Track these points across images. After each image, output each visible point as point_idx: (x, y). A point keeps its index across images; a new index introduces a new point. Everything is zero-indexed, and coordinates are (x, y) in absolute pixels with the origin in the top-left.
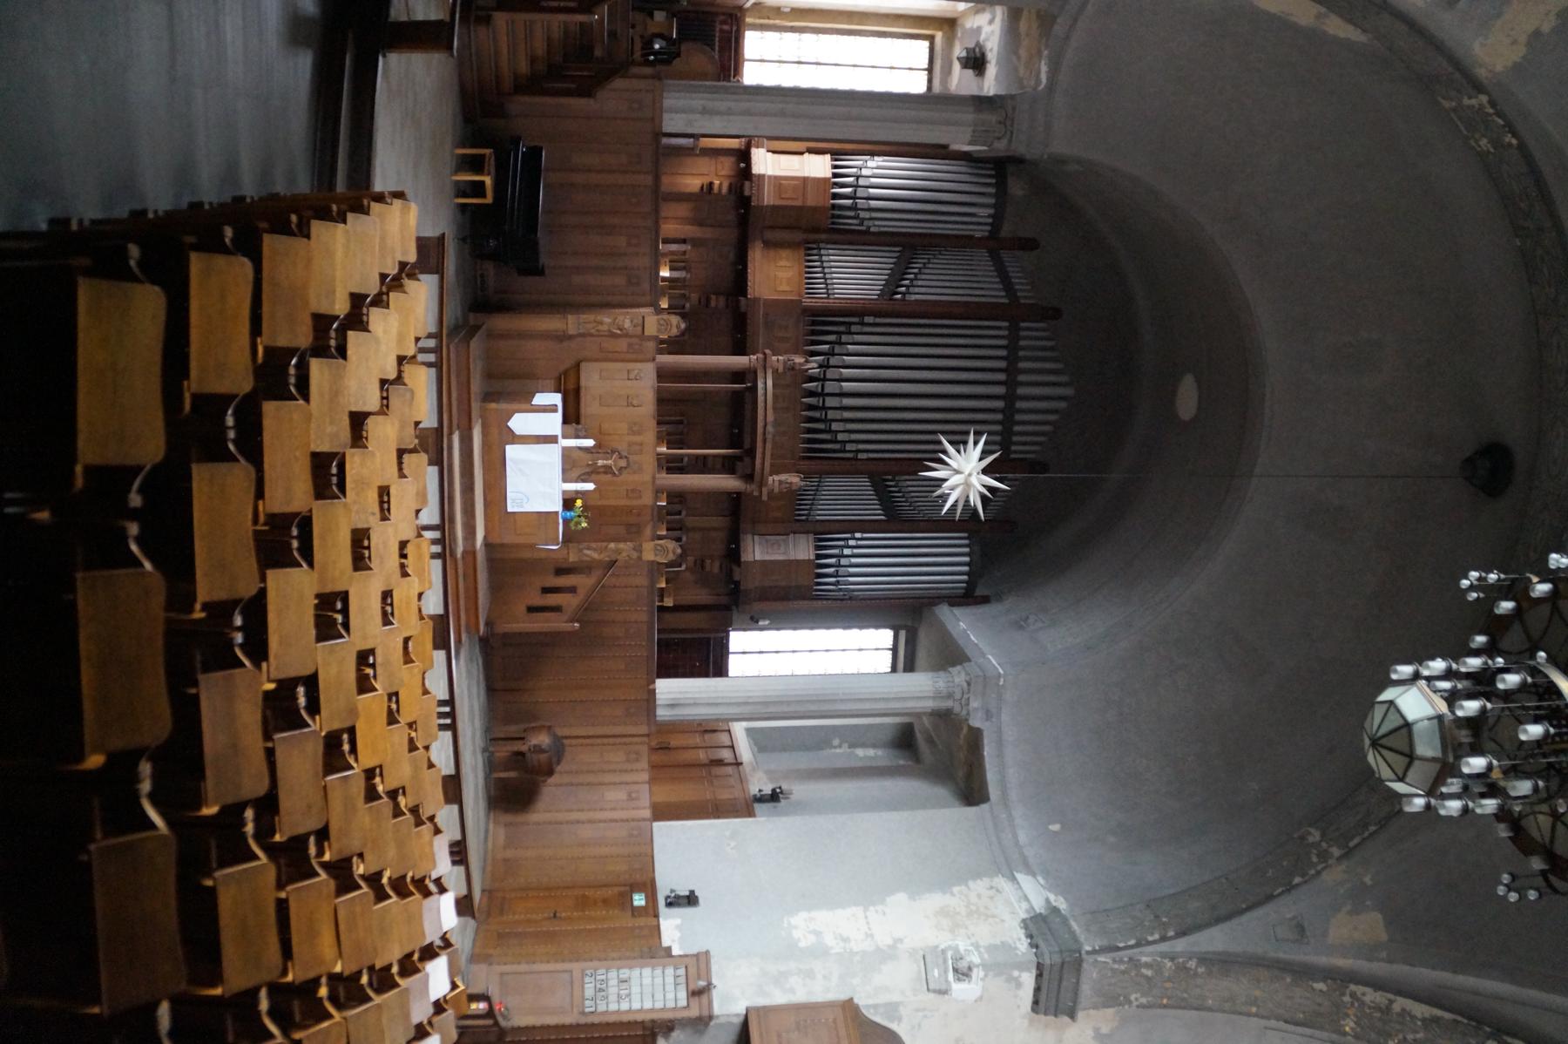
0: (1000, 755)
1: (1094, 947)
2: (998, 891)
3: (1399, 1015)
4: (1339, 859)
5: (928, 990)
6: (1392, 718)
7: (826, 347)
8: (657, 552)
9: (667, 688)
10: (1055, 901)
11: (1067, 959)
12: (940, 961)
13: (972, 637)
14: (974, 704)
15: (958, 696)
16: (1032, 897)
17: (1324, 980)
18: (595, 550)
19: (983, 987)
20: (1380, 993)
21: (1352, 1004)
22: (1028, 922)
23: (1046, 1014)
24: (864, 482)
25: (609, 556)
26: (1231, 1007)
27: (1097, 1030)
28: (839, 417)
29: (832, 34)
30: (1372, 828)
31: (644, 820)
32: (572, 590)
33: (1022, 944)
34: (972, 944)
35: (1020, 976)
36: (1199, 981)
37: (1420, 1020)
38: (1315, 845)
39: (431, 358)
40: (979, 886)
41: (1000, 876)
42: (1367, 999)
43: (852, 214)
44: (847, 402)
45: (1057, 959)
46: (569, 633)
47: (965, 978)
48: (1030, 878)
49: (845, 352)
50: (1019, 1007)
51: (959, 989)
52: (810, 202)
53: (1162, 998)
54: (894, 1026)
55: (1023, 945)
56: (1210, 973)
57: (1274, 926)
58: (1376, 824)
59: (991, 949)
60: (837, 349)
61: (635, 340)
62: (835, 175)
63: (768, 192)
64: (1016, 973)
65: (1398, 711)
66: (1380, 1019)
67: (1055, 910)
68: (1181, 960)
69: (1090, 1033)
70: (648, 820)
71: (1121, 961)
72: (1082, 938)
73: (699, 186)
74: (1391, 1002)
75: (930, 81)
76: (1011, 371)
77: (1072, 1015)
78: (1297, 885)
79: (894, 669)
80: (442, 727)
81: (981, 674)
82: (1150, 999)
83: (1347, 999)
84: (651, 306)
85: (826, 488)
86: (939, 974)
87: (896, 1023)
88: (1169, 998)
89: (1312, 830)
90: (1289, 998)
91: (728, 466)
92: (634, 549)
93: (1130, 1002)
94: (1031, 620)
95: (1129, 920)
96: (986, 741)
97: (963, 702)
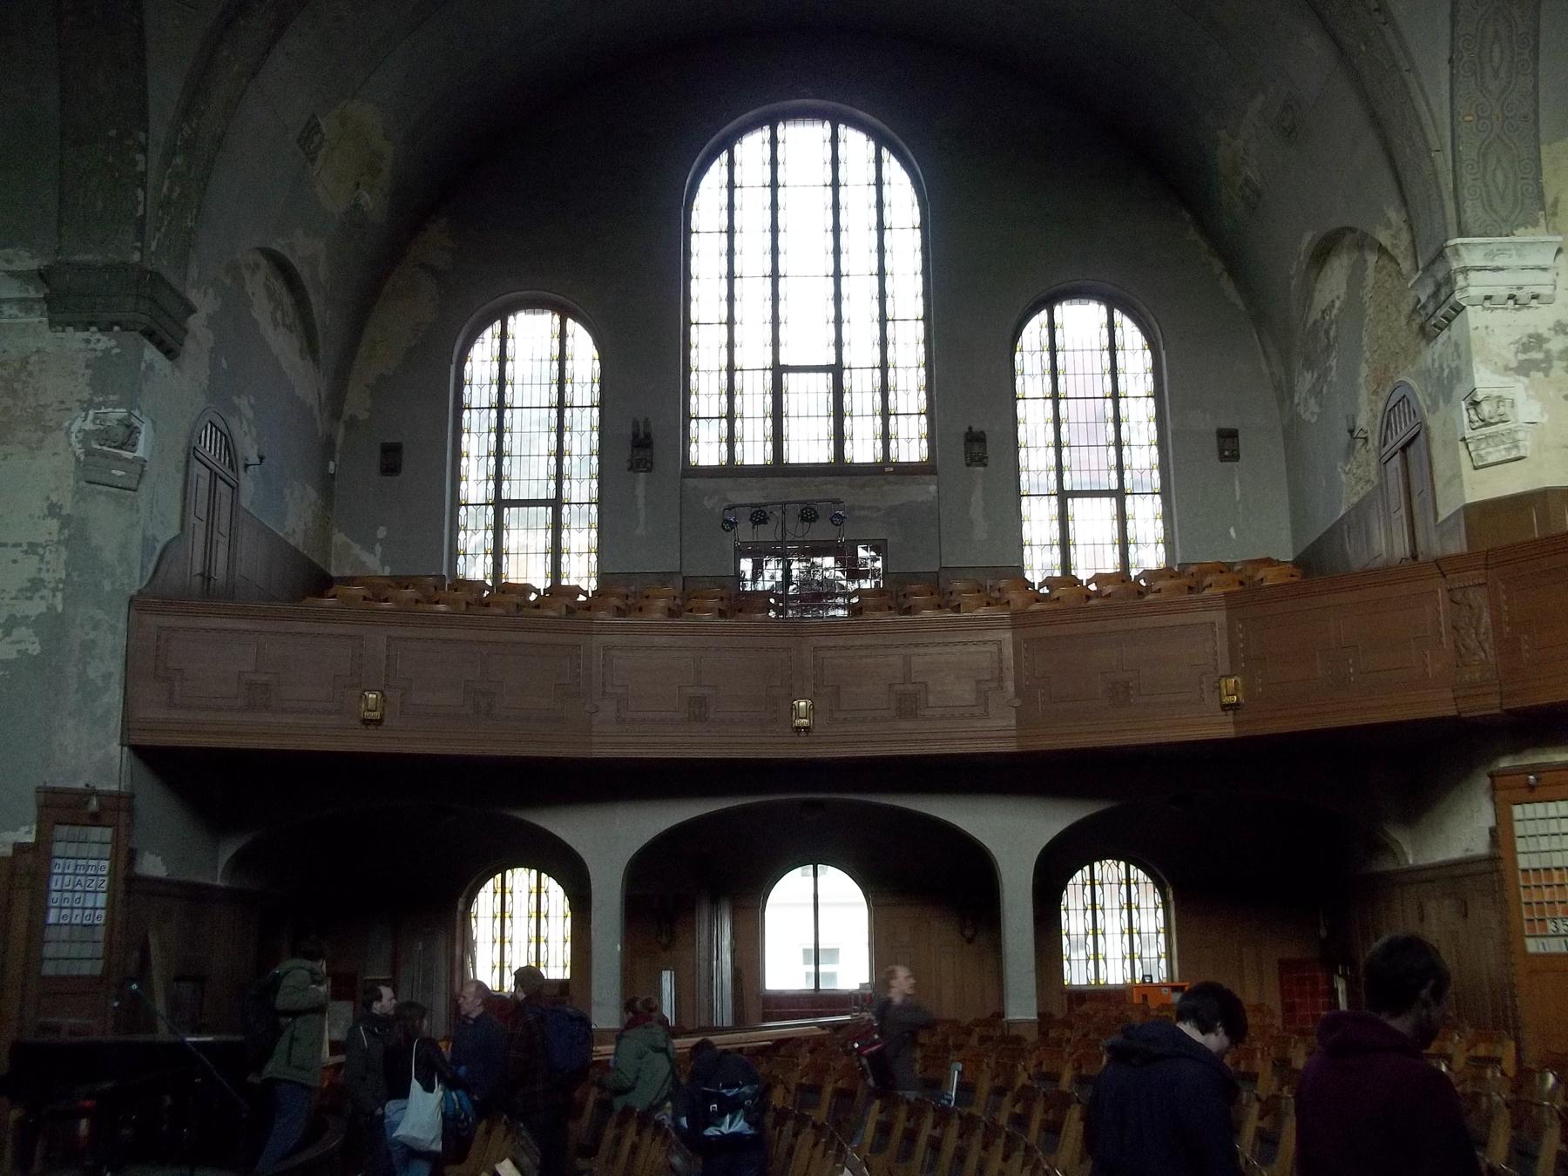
5: (135, 490)
29: (877, 193)
47: (133, 436)
54: (528, 582)
84: (1497, 823)
87: (156, 544)
95: (371, 206)
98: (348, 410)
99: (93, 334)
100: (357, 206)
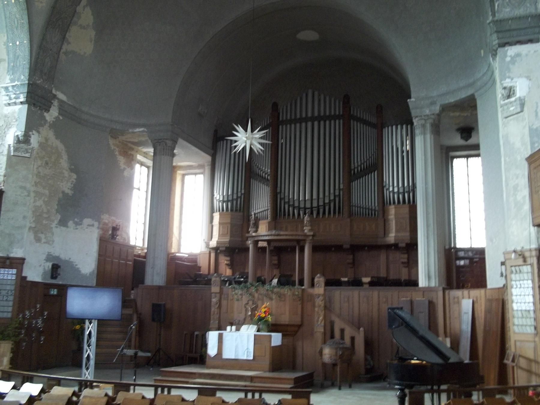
7: (291, 209)
8: (320, 286)
9: (422, 282)
12: (505, 107)
14: (427, 112)
15: (423, 122)
18: (319, 318)
19: (519, 77)
24: (354, 184)
25: (322, 311)
28: (322, 200)
31: (485, 292)
32: (342, 331)
39: (166, 390)
43: (235, 202)
44: (315, 196)
46: (365, 333)
47: (512, 90)
49: (292, 199)
50: (535, 52)
51: (519, 93)
52: (229, 221)
60: (291, 203)
61: (223, 296)
62: (219, 211)
63: (224, 239)
64: (508, 59)
70: (486, 291)
73: (229, 270)
75: (199, 173)
76: (301, 120)
79: (478, 155)
80: (169, 392)
85: (367, 204)
86: (512, 106)
91: (302, 250)
92: (318, 297)
96: (447, 102)
97: (426, 118)
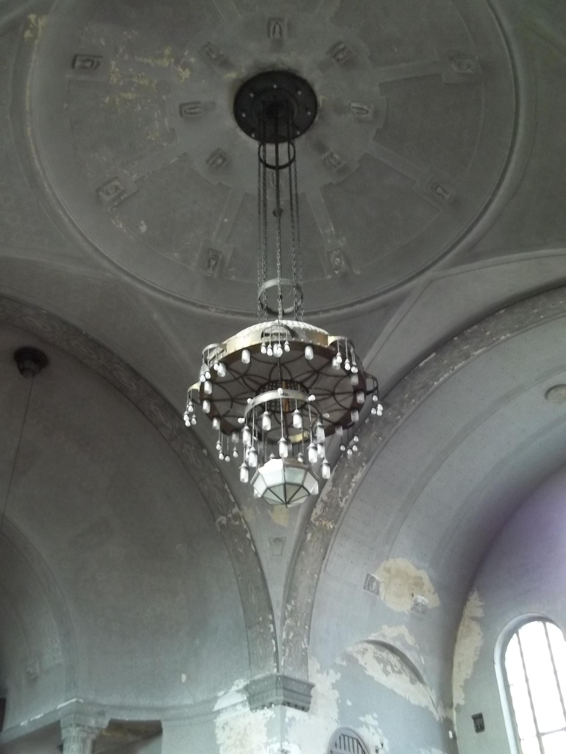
0: (130, 708)
1: (274, 667)
2: (227, 723)
3: (329, 498)
4: (240, 509)
6: (277, 490)
10: (238, 686)
11: (281, 685)
13: (38, 717)
14: (92, 723)
15: (84, 735)
16: (233, 701)
17: (306, 533)
20: (317, 505)
21: (321, 521)
22: (253, 707)
23: (309, 703)
26: (314, 588)
27: (318, 672)
30: (226, 487)
33: (268, 713)
34: (266, 747)
35: (288, 718)
36: (298, 605)
37: (333, 488)
38: (229, 520)
40: (221, 736)
41: (215, 720)
42: (319, 513)
45: (281, 691)
48: (219, 701)
53: (305, 628)
55: (268, 713)
56: (295, 598)
57: (273, 555)
58: (224, 484)
59: (269, 734)
65: (274, 486)
66: (330, 508)
67: (246, 688)
68: (286, 614)
69: (319, 676)
71: (284, 651)
72: (268, 673)
74: (322, 501)
77: (311, 686)
78: (251, 536)
81: (73, 716)
82: (305, 636)
83: (317, 524)
88: (305, 624)
89: (218, 520)
90: (313, 554)
93: (306, 649)
94: (31, 670)
95: (258, 641)
98: (455, 702)
99: (266, 710)
100: (416, 604)
